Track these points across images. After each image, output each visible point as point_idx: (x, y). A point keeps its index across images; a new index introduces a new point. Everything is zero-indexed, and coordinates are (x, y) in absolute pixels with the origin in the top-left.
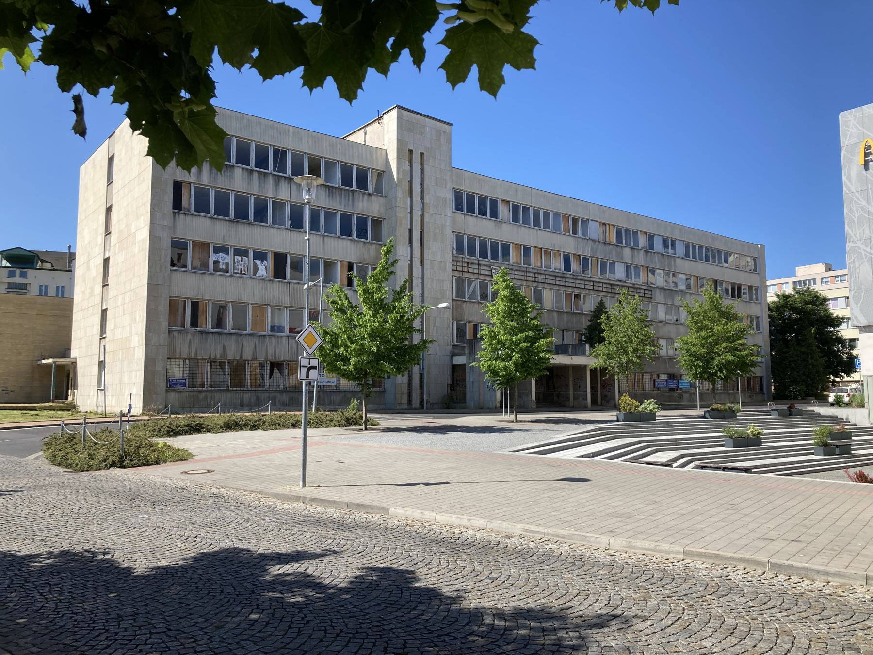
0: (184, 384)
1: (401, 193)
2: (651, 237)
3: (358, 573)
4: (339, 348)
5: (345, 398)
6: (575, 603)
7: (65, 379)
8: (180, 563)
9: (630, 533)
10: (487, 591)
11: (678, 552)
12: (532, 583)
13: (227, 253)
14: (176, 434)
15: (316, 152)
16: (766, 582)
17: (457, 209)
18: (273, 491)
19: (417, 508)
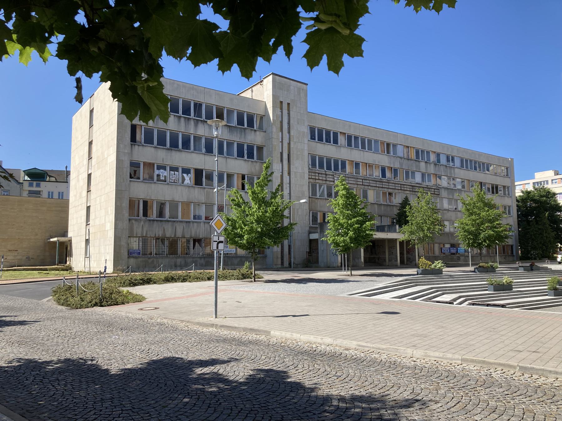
0: (139, 253)
1: (275, 129)
2: (438, 155)
3: (251, 373)
4: (237, 229)
5: (241, 261)
6: (391, 391)
7: (65, 250)
8: (139, 366)
9: (427, 347)
10: (334, 384)
11: (458, 359)
12: (363, 378)
13: (165, 170)
14: (135, 285)
15: (221, 104)
16: (516, 378)
17: (311, 139)
18: (197, 321)
19: (288, 331)
